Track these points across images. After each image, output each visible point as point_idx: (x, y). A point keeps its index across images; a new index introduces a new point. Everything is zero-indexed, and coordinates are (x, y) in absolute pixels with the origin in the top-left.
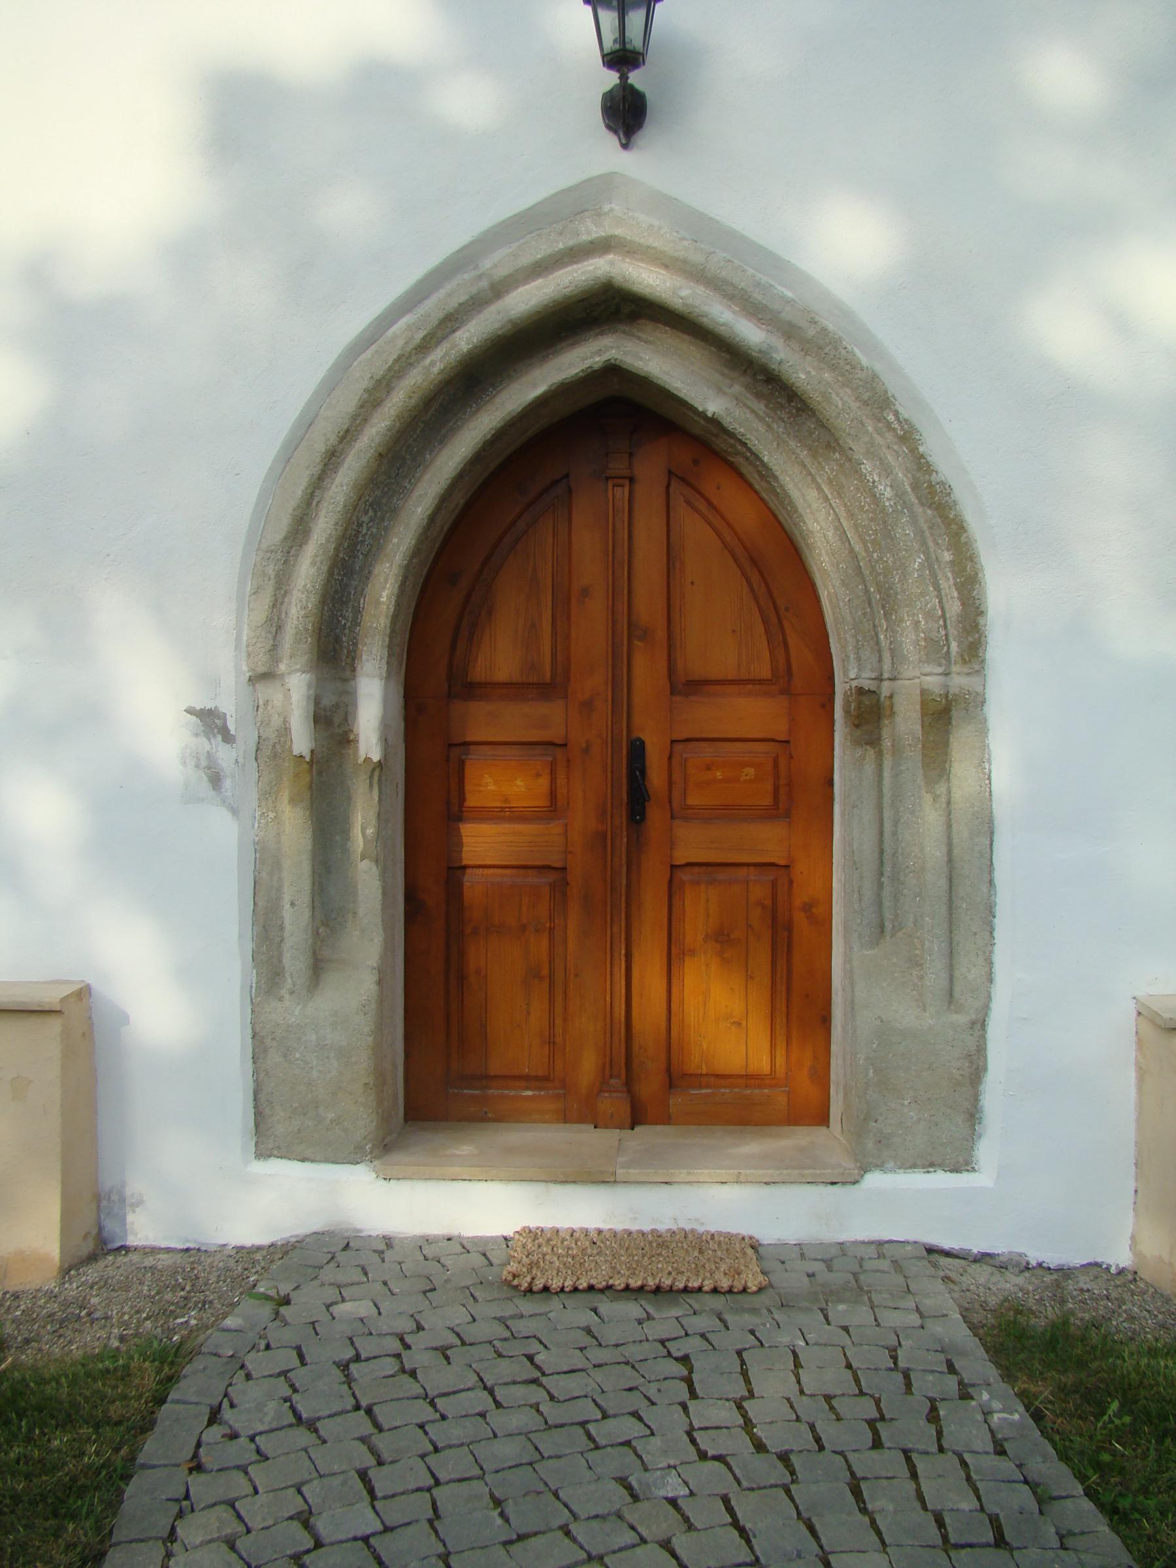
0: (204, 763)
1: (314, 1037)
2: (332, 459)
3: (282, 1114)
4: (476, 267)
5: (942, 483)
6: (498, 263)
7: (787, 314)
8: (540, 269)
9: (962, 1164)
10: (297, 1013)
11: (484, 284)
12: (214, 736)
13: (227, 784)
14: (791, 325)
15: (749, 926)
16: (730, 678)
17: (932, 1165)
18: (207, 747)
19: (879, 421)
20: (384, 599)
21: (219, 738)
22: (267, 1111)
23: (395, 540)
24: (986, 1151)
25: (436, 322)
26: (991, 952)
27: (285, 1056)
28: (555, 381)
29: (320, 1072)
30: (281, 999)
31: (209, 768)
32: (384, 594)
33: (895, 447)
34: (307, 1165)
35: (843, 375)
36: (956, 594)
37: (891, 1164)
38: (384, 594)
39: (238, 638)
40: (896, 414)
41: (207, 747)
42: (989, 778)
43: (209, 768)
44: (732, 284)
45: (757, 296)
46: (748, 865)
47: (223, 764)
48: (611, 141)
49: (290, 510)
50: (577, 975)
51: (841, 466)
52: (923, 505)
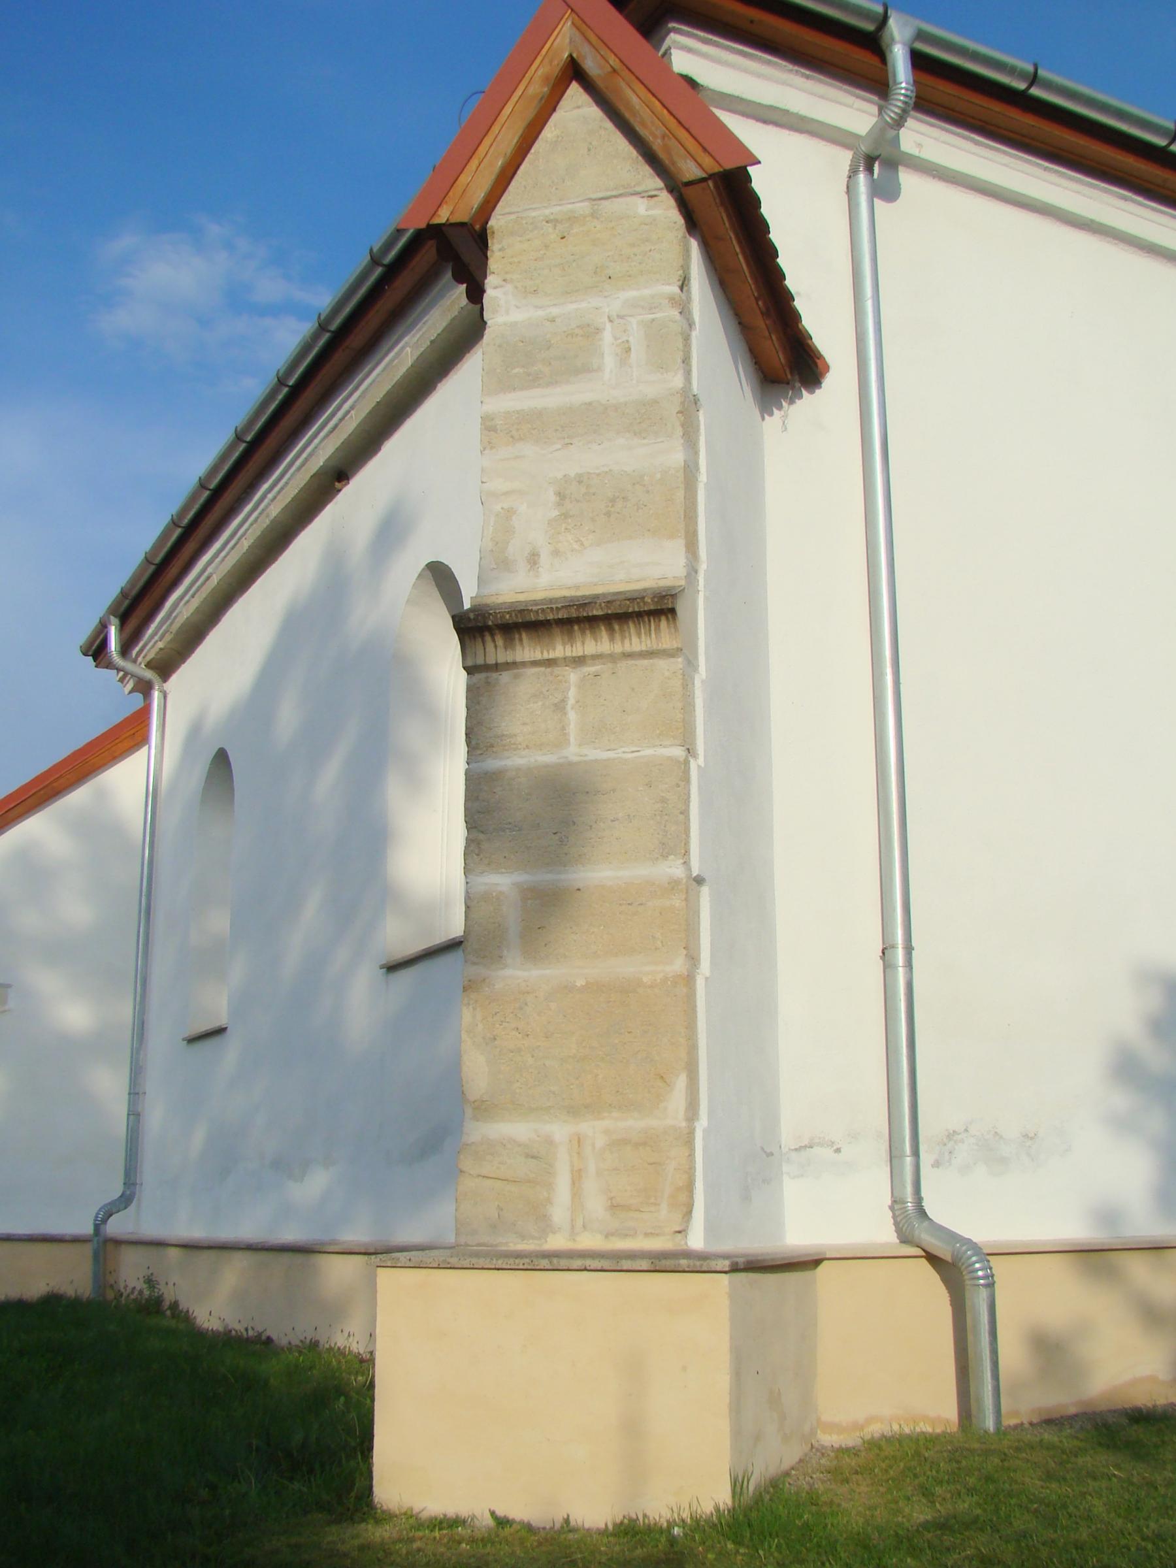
13: (633, 354)
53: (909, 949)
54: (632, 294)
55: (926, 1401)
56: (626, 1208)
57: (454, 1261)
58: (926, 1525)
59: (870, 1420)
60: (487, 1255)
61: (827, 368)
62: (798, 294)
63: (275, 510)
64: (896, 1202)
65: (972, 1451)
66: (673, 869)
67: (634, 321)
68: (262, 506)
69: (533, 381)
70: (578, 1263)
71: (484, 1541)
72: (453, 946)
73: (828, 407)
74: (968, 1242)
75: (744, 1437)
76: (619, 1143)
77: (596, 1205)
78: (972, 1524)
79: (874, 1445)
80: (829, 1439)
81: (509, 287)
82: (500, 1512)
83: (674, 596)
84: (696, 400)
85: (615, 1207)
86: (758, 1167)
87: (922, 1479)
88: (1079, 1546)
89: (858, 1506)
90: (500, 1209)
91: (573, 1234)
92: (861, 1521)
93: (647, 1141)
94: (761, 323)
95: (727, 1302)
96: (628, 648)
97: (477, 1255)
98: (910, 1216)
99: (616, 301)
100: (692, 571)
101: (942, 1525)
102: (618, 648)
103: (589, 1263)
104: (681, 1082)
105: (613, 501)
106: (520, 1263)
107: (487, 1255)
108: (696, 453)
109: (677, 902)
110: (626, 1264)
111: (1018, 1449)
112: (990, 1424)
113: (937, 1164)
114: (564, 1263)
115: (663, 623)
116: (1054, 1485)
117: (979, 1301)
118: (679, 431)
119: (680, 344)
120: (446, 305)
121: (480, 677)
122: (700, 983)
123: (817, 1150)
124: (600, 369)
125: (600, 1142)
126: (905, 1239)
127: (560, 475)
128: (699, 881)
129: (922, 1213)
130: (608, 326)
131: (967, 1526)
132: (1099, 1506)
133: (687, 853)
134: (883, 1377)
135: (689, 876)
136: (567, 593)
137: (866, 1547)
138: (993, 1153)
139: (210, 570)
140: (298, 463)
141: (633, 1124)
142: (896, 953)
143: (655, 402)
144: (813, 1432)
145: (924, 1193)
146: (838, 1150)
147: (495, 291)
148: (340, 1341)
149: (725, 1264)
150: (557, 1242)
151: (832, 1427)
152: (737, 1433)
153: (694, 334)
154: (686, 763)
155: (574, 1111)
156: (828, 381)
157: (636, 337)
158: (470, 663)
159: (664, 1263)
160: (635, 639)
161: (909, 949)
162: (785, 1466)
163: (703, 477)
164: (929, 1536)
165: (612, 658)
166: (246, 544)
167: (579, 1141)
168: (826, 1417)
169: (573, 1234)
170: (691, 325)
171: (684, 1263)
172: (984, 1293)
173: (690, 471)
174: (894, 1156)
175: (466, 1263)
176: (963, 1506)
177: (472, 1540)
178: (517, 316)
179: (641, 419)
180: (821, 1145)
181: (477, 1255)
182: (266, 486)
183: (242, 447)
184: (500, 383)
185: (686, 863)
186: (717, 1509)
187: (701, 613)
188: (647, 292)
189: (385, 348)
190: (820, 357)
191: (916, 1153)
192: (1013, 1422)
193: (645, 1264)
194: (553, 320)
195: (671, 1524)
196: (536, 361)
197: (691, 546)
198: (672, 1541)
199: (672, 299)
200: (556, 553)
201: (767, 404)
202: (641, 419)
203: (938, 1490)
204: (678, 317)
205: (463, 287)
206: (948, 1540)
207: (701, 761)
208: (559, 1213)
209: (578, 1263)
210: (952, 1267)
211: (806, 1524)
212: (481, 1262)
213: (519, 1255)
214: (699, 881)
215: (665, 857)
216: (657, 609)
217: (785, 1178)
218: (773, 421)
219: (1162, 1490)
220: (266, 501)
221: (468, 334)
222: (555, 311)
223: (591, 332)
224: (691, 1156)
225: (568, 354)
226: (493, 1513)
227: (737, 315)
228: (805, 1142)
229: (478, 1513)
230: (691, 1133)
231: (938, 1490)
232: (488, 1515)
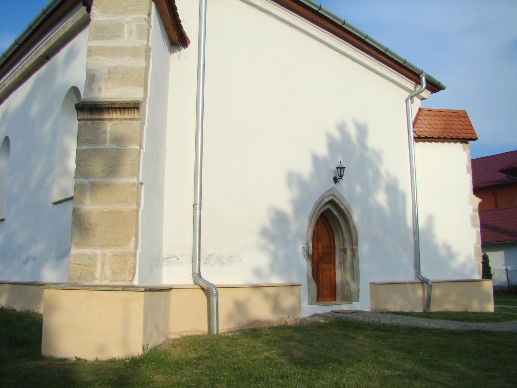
2: (312, 217)
9: (358, 301)
13: (133, 33)
24: (360, 299)
53: (201, 205)
54: (134, 16)
55: (199, 326)
56: (117, 274)
57: (67, 287)
58: (194, 358)
59: (183, 331)
60: (76, 286)
61: (190, 42)
62: (183, 21)
63: (27, 66)
64: (194, 273)
65: (209, 339)
66: (134, 180)
67: (134, 24)
68: (23, 64)
69: (103, 38)
70: (102, 288)
71: (72, 364)
72: (71, 199)
73: (189, 53)
74: (212, 284)
75: (146, 335)
76: (115, 256)
77: (108, 272)
78: (206, 358)
79: (184, 338)
80: (172, 337)
81: (98, 10)
82: (78, 357)
83: (139, 104)
84: (150, 48)
85: (113, 273)
86: (156, 262)
87: (195, 346)
88: (233, 363)
89: (177, 354)
90: (81, 273)
91: (101, 281)
92: (177, 357)
93: (123, 255)
94: (171, 28)
95: (143, 300)
96: (125, 117)
97: (73, 286)
98: (197, 277)
99: (129, 18)
100: (145, 97)
101: (199, 358)
102: (122, 117)
103: (105, 288)
104: (133, 239)
105: (124, 75)
106: (85, 288)
107: (76, 286)
108: (149, 63)
109: (135, 189)
110: (116, 289)
111: (221, 339)
112: (215, 332)
113: (205, 263)
114: (98, 288)
115: (136, 111)
116: (229, 348)
117: (214, 300)
118: (144, 57)
119: (147, 32)
120: (80, 13)
121: (82, 122)
122: (140, 212)
123: (172, 259)
124: (123, 37)
125: (110, 255)
126: (196, 283)
127: (109, 66)
128: (142, 184)
129: (200, 276)
130: (126, 25)
131: (205, 358)
132: (240, 353)
133: (138, 176)
134: (187, 320)
135: (139, 182)
136: (109, 100)
137: (178, 364)
138: (220, 261)
139: (5, 82)
140: (35, 53)
141: (119, 250)
142: (197, 206)
143: (138, 48)
144: (168, 335)
145: (201, 271)
146: (178, 259)
147: (94, 10)
148: (36, 310)
149: (143, 289)
150: (97, 283)
151: (173, 333)
152: (145, 334)
153: (151, 30)
154: (140, 151)
155: (103, 246)
156: (190, 46)
157: (134, 29)
158: (79, 118)
159: (126, 289)
160: (127, 115)
161: (201, 205)
162: (159, 344)
163: (150, 70)
164: (194, 361)
165: (121, 119)
166: (17, 75)
167: (104, 255)
168: (172, 331)
169: (101, 281)
170: (150, 27)
171: (132, 289)
172: (215, 298)
173: (147, 69)
174: (194, 261)
175: (70, 288)
176: (204, 353)
177: (69, 364)
178: (100, 19)
179: (133, 52)
180: (174, 257)
181: (73, 286)
182: (24, 58)
183: (17, 46)
184: (94, 37)
185: (138, 179)
186: (138, 355)
187: (147, 109)
188: (138, 16)
189: (62, 21)
190: (188, 39)
191: (199, 260)
192: (222, 332)
193: (121, 289)
194: (110, 21)
195: (126, 359)
196: (104, 32)
197: (146, 90)
198: (125, 363)
199: (145, 19)
200: (107, 88)
201: (172, 51)
202: (133, 52)
203: (199, 349)
204: (147, 24)
205: (86, 8)
206: (200, 362)
207: (144, 150)
208: (98, 273)
209: (102, 288)
210: (208, 291)
211: (162, 359)
212: (75, 288)
213: (86, 286)
214: (142, 184)
215: (132, 176)
216: (134, 107)
217: (163, 266)
218: (176, 54)
219: (257, 348)
220: (24, 63)
221: (85, 22)
222: (111, 18)
223: (121, 26)
224: (135, 260)
225: (114, 31)
226: (76, 357)
227: (165, 25)
228: (169, 256)
229: (72, 357)
230: (136, 253)
231: (199, 349)
232: (74, 357)
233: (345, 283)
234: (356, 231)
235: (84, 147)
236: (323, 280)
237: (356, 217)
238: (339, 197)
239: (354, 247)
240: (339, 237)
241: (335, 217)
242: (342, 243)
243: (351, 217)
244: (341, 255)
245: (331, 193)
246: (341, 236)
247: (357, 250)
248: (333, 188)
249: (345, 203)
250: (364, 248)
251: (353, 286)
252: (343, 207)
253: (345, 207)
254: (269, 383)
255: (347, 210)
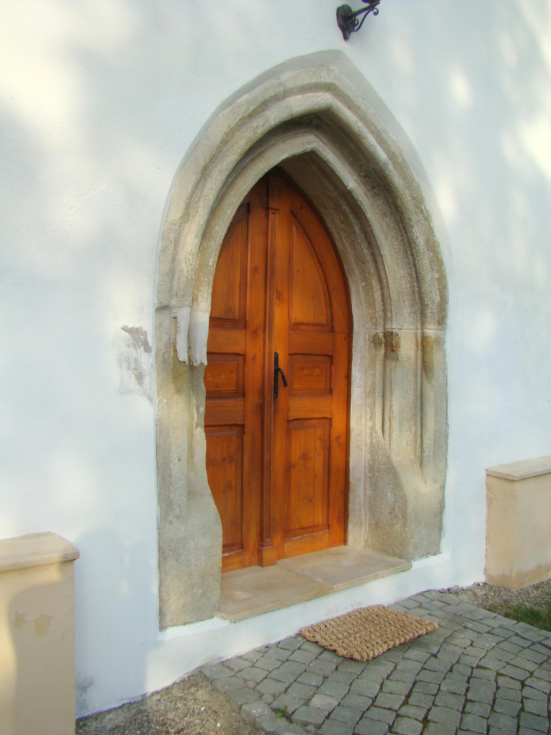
0: (133, 366)
1: (193, 544)
2: (205, 172)
3: (174, 598)
4: (278, 78)
5: (437, 242)
6: (288, 79)
7: (393, 148)
8: (304, 89)
10: (183, 530)
11: (281, 89)
12: (139, 347)
13: (147, 380)
14: (393, 154)
15: (316, 450)
16: (304, 322)
17: (428, 554)
18: (135, 354)
19: (418, 208)
20: (211, 264)
21: (142, 348)
22: (166, 598)
23: (217, 228)
24: (445, 543)
25: (259, 103)
26: (447, 454)
27: (177, 560)
28: (292, 153)
29: (196, 565)
30: (171, 522)
31: (136, 369)
32: (211, 261)
33: (422, 222)
34: (188, 626)
35: (408, 183)
36: (438, 293)
37: (417, 557)
38: (211, 261)
39: (155, 281)
40: (425, 207)
41: (135, 354)
42: (447, 377)
43: (136, 369)
44: (375, 127)
45: (384, 136)
46: (315, 418)
47: (145, 367)
48: (339, 33)
49: (185, 199)
50: (248, 484)
51: (388, 225)
52: (429, 250)
233: (384, 472)
234: (438, 262)
235: (226, 554)
236: (289, 468)
237: (446, 199)
238: (358, 101)
239: (431, 331)
240: (369, 288)
241: (347, 195)
242: (380, 314)
243: (419, 201)
244: (373, 361)
245: (326, 78)
246: (375, 284)
247: (440, 341)
248: (335, 56)
249: (392, 137)
250: (472, 332)
251: (418, 487)
252: (382, 155)
253: (392, 156)
254: (382, 636)
255: (401, 166)
